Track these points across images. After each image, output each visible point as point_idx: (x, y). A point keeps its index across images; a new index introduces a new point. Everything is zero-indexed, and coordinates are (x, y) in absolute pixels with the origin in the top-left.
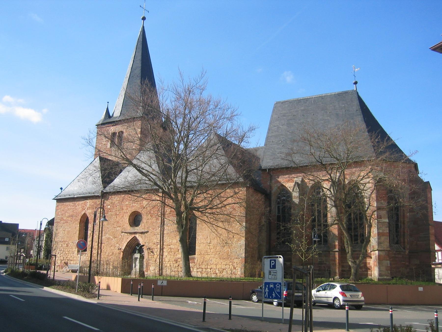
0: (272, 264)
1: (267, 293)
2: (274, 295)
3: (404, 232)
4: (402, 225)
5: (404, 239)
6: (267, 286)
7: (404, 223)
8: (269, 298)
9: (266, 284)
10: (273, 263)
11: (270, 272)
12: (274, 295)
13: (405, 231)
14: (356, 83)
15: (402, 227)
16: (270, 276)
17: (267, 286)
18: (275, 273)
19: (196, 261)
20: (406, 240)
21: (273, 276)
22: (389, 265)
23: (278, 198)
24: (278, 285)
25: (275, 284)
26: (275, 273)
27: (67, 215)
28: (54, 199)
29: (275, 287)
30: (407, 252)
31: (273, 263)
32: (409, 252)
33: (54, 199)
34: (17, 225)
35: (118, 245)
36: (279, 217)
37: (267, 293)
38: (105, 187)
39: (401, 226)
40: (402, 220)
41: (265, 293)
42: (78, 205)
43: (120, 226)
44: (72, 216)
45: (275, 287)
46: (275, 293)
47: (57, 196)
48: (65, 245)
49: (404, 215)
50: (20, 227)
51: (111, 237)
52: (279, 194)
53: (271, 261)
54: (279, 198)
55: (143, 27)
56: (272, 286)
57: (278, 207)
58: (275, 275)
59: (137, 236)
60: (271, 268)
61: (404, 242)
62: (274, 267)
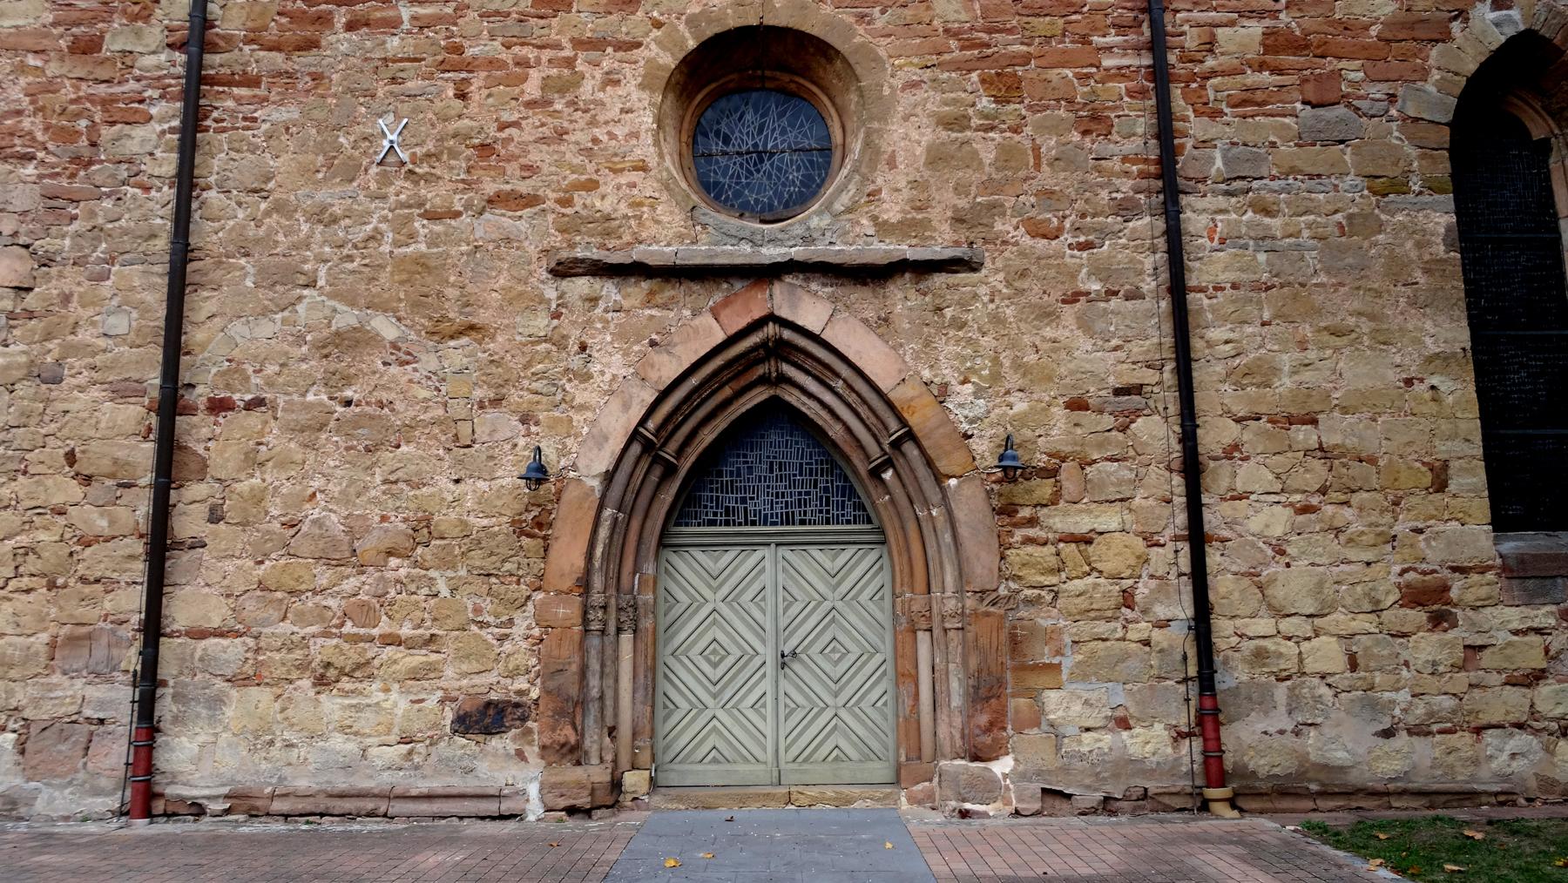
51: (386, 328)
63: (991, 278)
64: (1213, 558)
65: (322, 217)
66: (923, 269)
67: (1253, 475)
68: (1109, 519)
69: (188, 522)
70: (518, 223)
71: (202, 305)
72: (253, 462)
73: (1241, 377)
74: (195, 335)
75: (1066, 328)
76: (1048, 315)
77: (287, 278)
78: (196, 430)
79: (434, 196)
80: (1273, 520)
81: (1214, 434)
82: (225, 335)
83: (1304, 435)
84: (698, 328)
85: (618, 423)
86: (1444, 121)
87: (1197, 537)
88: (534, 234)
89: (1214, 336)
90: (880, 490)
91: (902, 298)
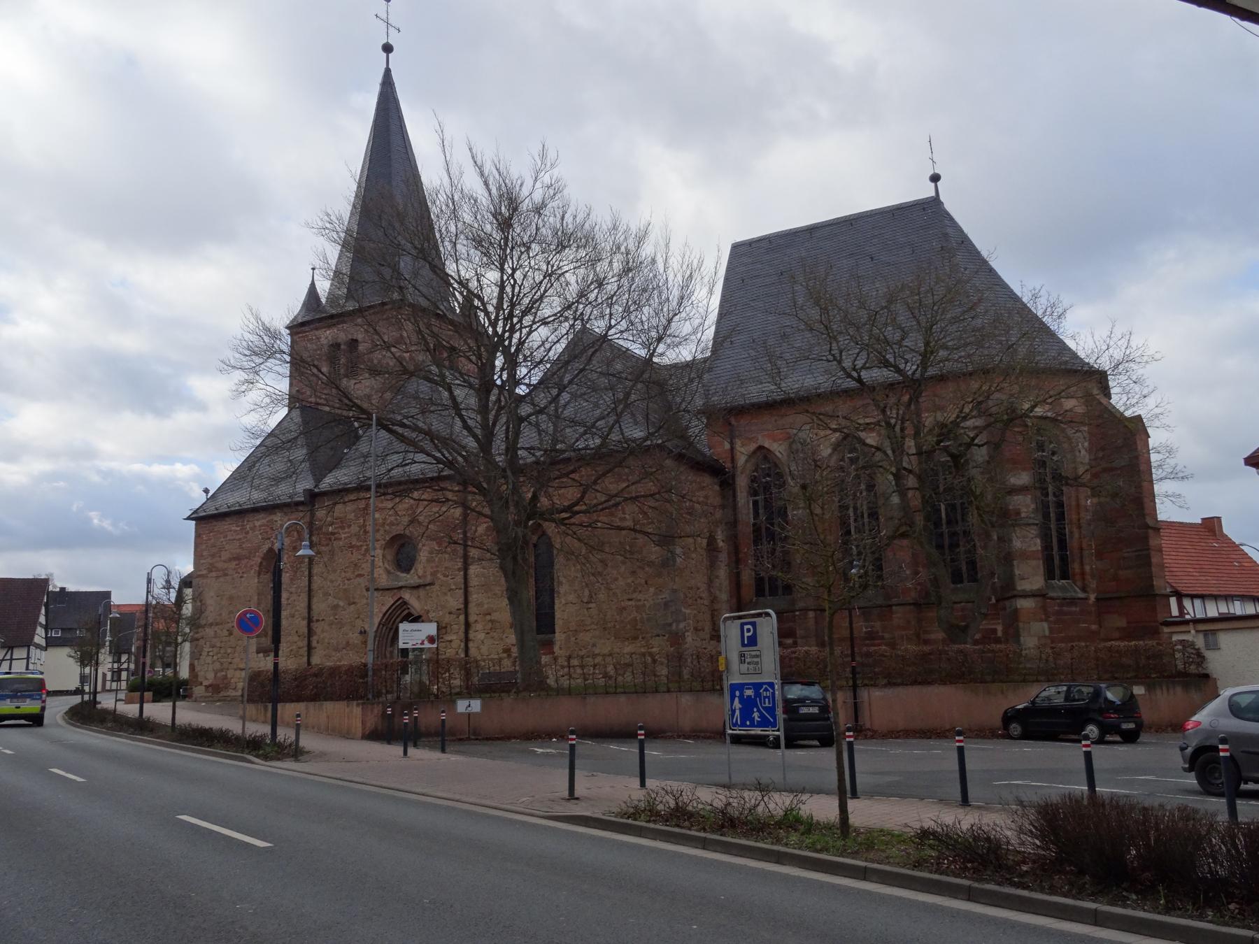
0: (746, 634)
1: (738, 712)
2: (756, 715)
3: (1081, 549)
4: (1075, 530)
5: (1082, 564)
6: (737, 693)
7: (1079, 527)
8: (743, 724)
9: (734, 688)
10: (749, 630)
11: (742, 656)
12: (756, 715)
13: (1084, 545)
14: (935, 178)
15: (1076, 535)
16: (744, 667)
17: (737, 693)
18: (757, 656)
19: (556, 649)
20: (1087, 568)
21: (751, 667)
22: (1047, 633)
23: (752, 481)
24: (766, 690)
25: (757, 686)
26: (757, 656)
27: (225, 555)
28: (189, 518)
29: (757, 694)
30: (1092, 597)
31: (749, 630)
32: (1097, 599)
33: (189, 518)
34: (107, 595)
35: (359, 623)
36: (757, 529)
37: (738, 712)
38: (318, 481)
39: (1071, 532)
40: (1074, 517)
41: (733, 712)
42: (253, 529)
43: (360, 576)
44: (238, 558)
45: (757, 694)
46: (759, 711)
47: (195, 512)
48: (226, 633)
49: (1078, 505)
50: (115, 600)
51: (341, 604)
52: (756, 470)
53: (742, 625)
54: (754, 480)
55: (388, 72)
56: (749, 692)
57: (755, 503)
58: (757, 663)
59: (407, 596)
60: (743, 645)
61: (1083, 574)
62: (753, 641)
63: (436, 587)
64: (471, 644)
65: (332, 581)
66: (425, 585)
67: (479, 626)
68: (454, 637)
69: (314, 644)
70: (360, 580)
71: (315, 600)
72: (323, 631)
73: (478, 605)
74: (314, 607)
75: (449, 598)
76: (445, 594)
77: (326, 594)
78: (314, 625)
79: (348, 575)
80: (481, 636)
81: (472, 619)
82: (319, 606)
83: (488, 617)
84: (389, 601)
85: (377, 621)
86: (473, 651)
87: (467, 640)
88: (363, 582)
89: (474, 597)
90: (687, 309)
91: (422, 592)
